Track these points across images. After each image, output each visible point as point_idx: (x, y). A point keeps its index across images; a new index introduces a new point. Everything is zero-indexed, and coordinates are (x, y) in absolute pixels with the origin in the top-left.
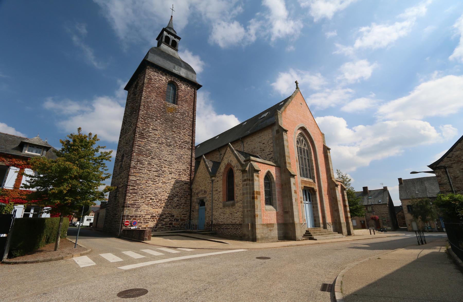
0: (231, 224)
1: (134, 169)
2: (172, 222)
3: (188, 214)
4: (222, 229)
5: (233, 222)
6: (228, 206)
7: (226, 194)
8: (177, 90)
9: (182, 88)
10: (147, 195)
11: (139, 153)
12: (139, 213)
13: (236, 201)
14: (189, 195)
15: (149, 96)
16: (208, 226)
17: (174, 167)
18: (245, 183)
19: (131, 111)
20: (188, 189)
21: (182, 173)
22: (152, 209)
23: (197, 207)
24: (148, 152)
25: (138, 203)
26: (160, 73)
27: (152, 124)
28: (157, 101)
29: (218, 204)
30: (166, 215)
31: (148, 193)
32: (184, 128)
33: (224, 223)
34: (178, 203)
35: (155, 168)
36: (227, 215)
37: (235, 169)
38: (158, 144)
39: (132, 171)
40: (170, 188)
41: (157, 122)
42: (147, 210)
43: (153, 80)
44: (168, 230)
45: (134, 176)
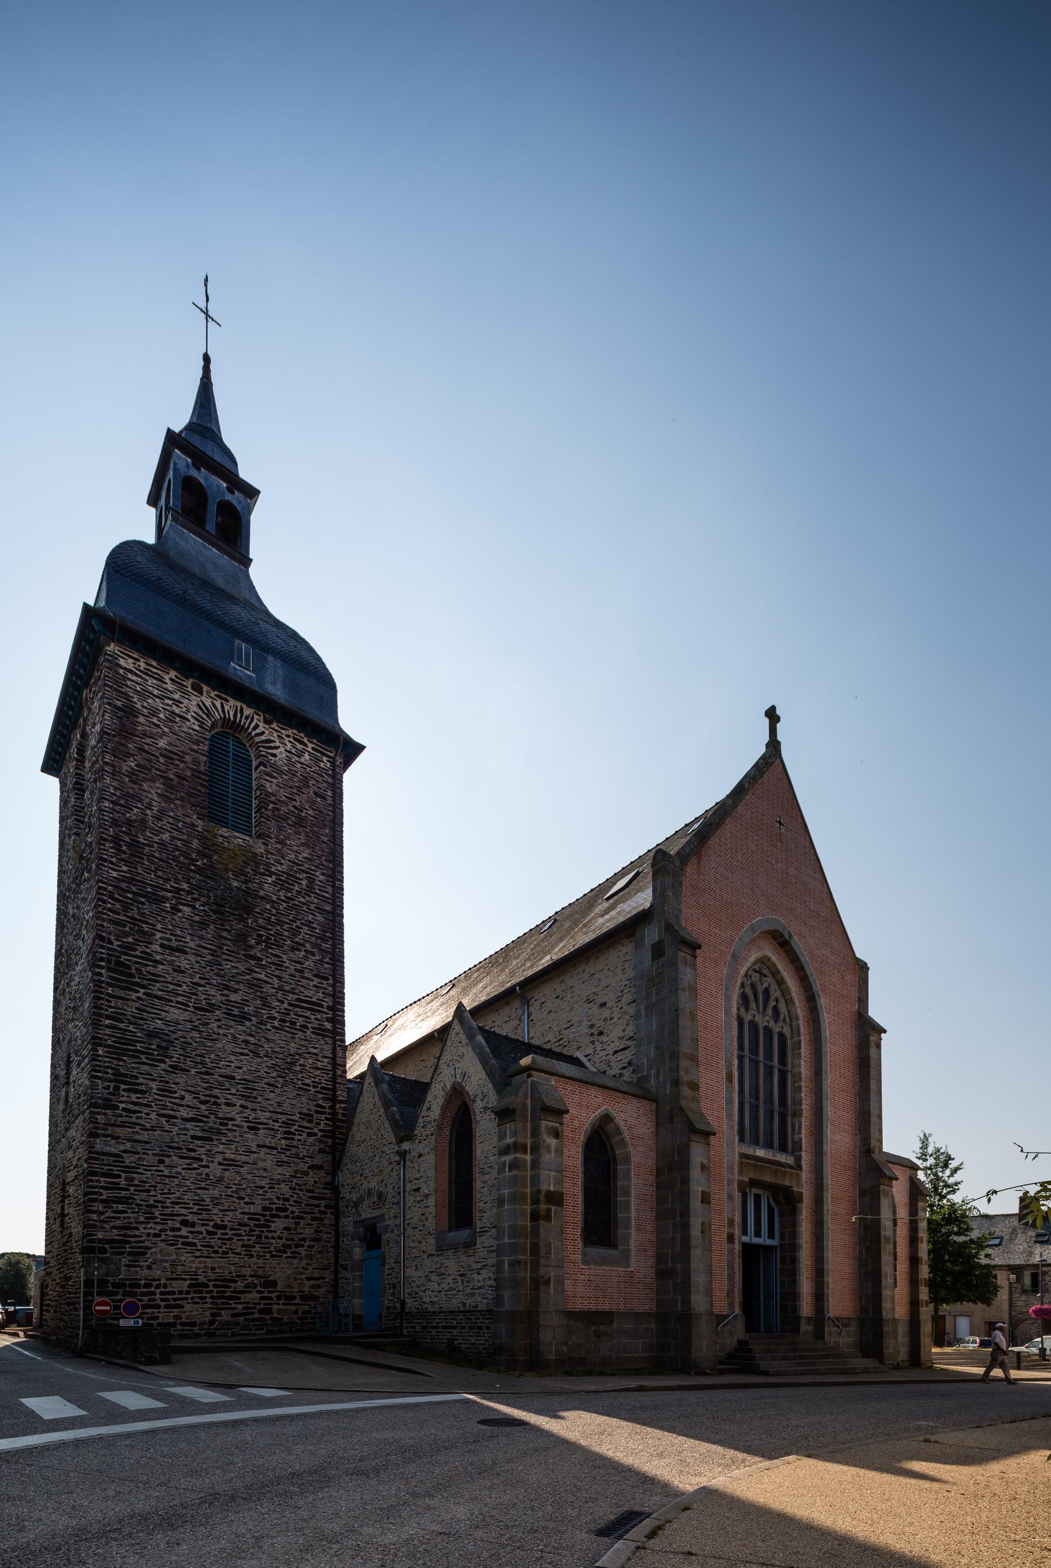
0: (460, 1312)
1: (107, 1111)
2: (271, 1304)
3: (329, 1276)
4: (434, 1327)
5: (467, 1305)
6: (454, 1247)
7: (450, 1203)
8: (254, 766)
9: (275, 755)
10: (168, 1207)
11: (119, 1048)
12: (146, 1272)
13: (478, 1230)
14: (328, 1211)
15: (132, 796)
16: (391, 1320)
17: (264, 1104)
18: (505, 1161)
19: (77, 868)
20: (324, 1188)
21: (296, 1127)
22: (193, 1258)
23: (358, 1252)
24: (155, 1041)
25: (135, 1236)
26: (171, 679)
27: (159, 927)
28: (171, 820)
29: (420, 1242)
30: (246, 1282)
31: (171, 1203)
32: (297, 943)
33: (441, 1308)
34: (287, 1240)
35: (188, 1106)
36: (450, 1279)
37: (478, 1106)
38: (192, 1009)
39: (99, 1117)
40: (254, 1183)
41: (180, 914)
42: (174, 1265)
43: (141, 719)
44: (257, 1332)
45: (109, 1139)
